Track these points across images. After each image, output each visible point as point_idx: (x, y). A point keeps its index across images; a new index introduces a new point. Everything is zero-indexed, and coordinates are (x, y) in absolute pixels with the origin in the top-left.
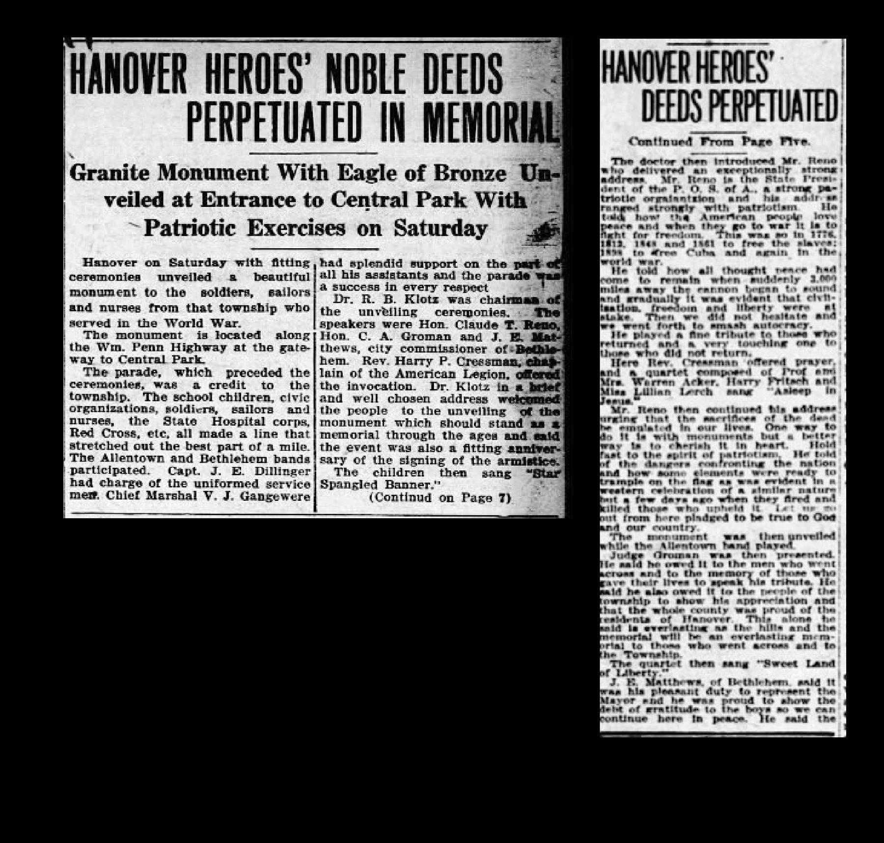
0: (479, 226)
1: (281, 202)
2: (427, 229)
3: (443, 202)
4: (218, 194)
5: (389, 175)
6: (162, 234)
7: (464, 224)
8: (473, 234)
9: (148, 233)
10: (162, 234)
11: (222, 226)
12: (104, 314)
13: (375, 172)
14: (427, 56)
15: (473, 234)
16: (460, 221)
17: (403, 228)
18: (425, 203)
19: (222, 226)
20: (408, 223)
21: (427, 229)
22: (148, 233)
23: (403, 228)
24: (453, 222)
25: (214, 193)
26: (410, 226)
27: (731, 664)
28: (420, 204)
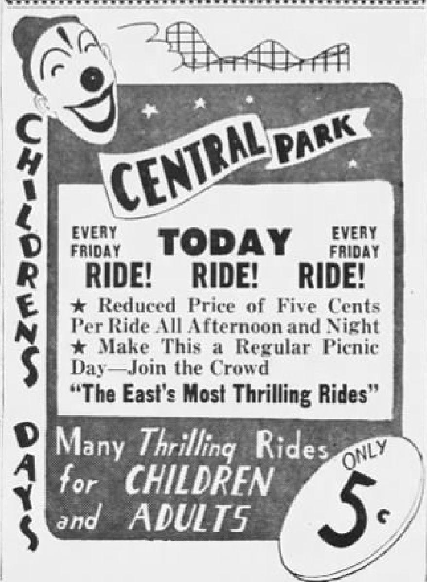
0: (273, 233)
7: (349, 389)
9: (326, 352)
13: (357, 324)
22: (326, 352)
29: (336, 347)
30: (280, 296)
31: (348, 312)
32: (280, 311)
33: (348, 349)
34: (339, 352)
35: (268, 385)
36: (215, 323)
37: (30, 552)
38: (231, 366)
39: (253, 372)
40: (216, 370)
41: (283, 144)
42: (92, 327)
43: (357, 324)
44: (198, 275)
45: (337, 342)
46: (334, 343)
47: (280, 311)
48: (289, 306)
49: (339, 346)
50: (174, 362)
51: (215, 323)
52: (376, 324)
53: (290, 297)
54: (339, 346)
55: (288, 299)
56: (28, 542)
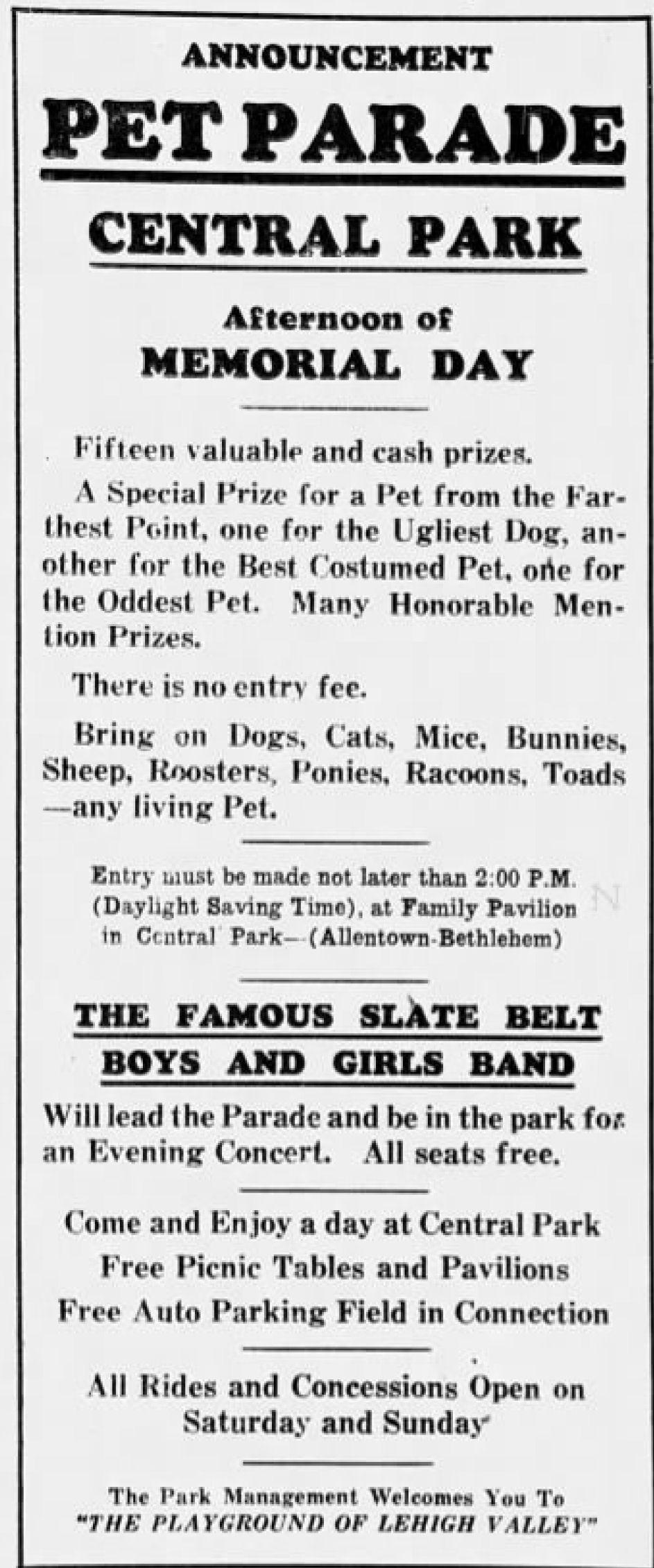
1: (355, 58)
2: (228, 1424)
3: (569, 1228)
4: (79, 1303)
5: (522, 608)
6: (465, 1276)
7: (454, 1418)
8: (354, 1231)
10: (465, 1276)
11: (572, 1312)
12: (138, 1512)
13: (429, 529)
14: (108, 1055)
15: (354, 1231)
16: (449, 1413)
17: (195, 1423)
18: (544, 1229)
19: (572, 1312)
20: (202, 1415)
21: (228, 1424)
23: (195, 1423)
24: (265, 1414)
25: (74, 1301)
26: (205, 1420)
27: (119, 1385)
28: (537, 1232)
29: (196, 1268)
30: (342, 1298)
31: (126, 1125)
32: (106, 1273)
33: (214, 1271)
34: (201, 1274)
35: (500, 1258)
36: (121, 446)
37: (38, 173)
38: (457, 493)
39: (385, 1500)
40: (335, 740)
41: (392, 123)
42: (295, 1153)
43: (429, 529)
44: (112, 1062)
45: (198, 1260)
46: (193, 1262)
47: (106, 1273)
48: (356, 1313)
49: (201, 1266)
50: (460, 1110)
51: (121, 446)
52: (193, 903)
53: (357, 1299)
54: (201, 1266)
55: (354, 1303)
56: (489, 1500)
